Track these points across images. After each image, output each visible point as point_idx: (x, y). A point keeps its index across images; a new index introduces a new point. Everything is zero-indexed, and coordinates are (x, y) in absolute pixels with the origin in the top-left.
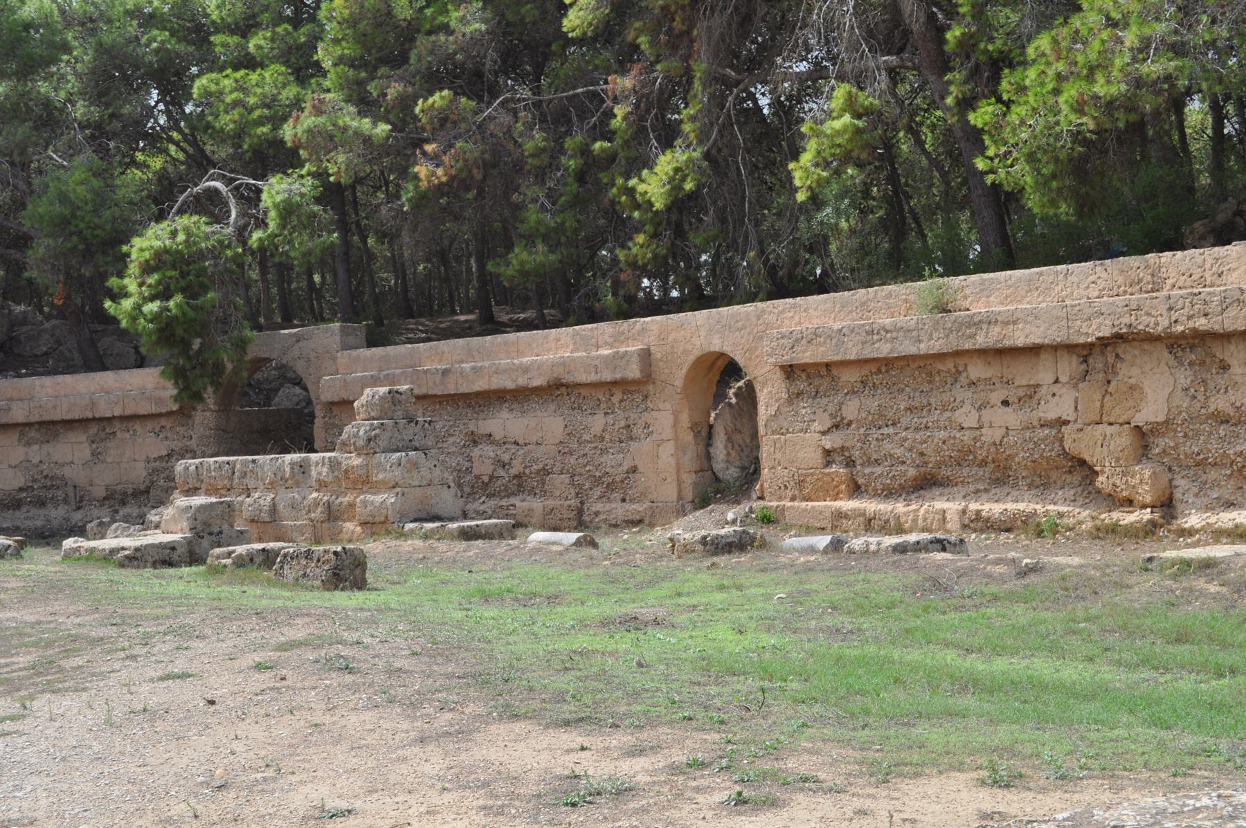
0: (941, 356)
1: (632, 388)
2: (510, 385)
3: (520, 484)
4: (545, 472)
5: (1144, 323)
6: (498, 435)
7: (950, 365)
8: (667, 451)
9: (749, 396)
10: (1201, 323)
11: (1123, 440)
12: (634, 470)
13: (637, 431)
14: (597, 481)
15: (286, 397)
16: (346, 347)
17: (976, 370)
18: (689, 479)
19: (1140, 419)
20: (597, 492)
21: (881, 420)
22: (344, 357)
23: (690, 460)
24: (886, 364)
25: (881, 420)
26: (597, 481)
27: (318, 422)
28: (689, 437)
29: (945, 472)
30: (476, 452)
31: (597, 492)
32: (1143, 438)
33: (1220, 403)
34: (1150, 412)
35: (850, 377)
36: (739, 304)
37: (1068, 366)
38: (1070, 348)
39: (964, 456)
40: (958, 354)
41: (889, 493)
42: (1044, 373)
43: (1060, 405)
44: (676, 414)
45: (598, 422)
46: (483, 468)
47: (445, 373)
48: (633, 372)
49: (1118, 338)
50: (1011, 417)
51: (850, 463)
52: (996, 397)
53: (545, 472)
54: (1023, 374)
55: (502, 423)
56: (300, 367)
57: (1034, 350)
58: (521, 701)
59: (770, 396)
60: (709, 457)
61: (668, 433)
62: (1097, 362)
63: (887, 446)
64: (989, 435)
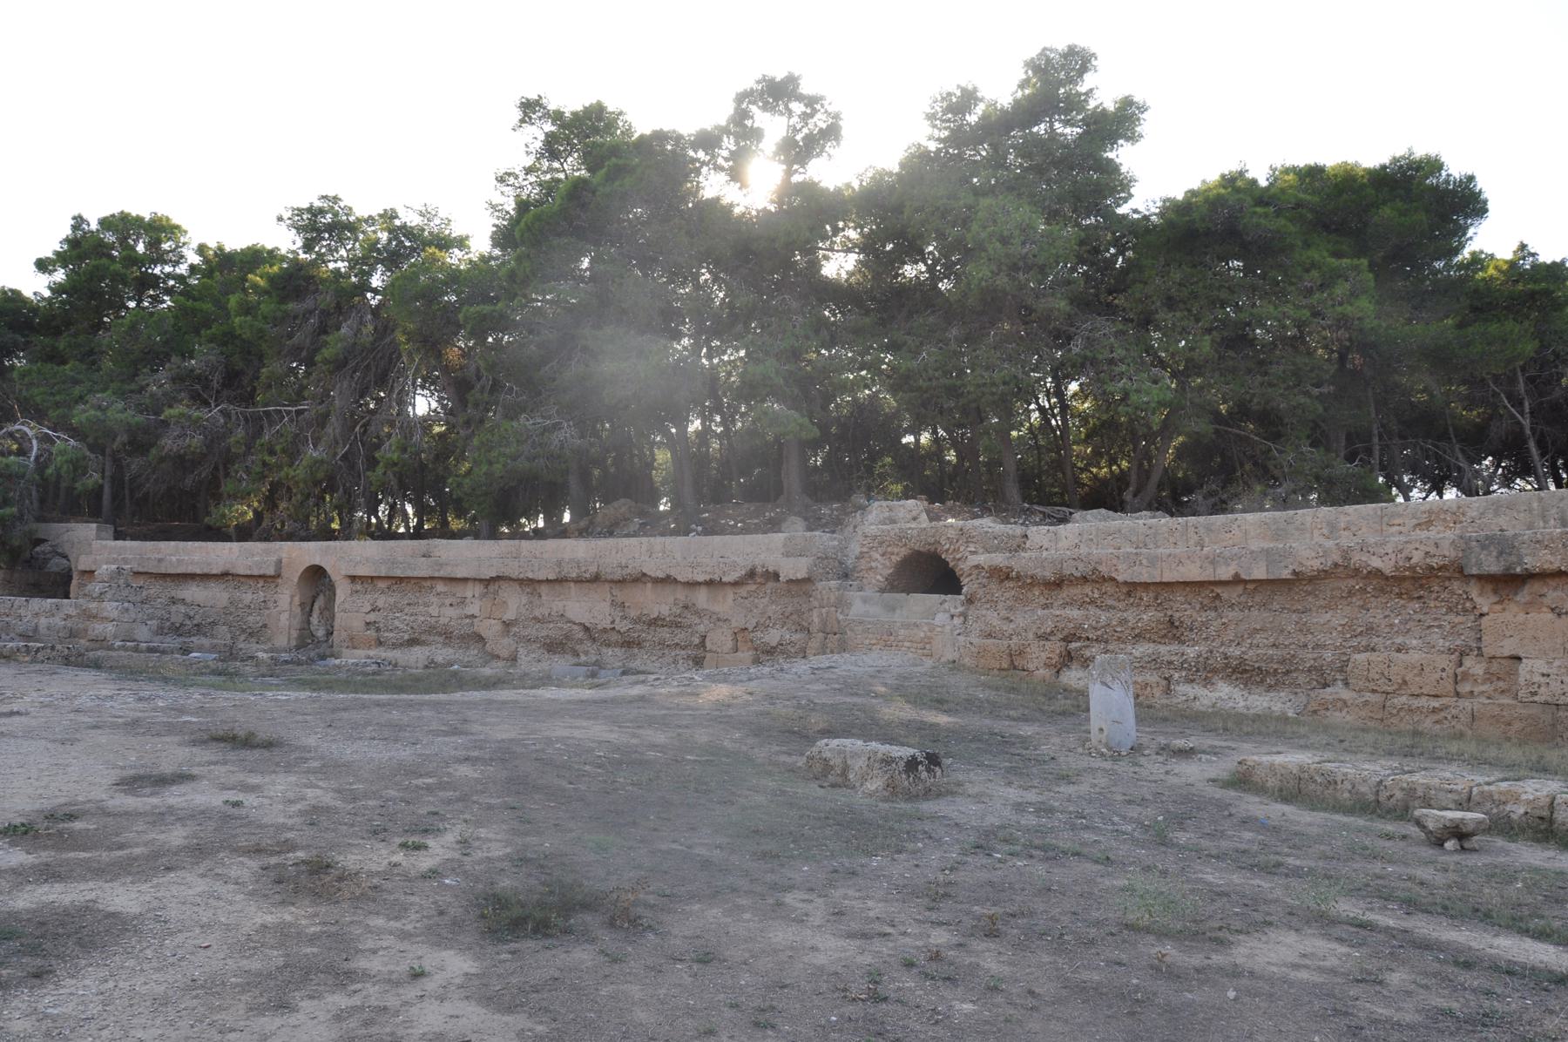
0: (424, 579)
1: (271, 579)
2: (198, 571)
3: (199, 629)
4: (214, 623)
5: (508, 572)
6: (189, 600)
7: (428, 583)
8: (284, 617)
9: (331, 588)
10: (530, 575)
11: (497, 627)
12: (265, 626)
13: (271, 604)
14: (244, 631)
15: (56, 564)
16: (98, 538)
17: (440, 587)
18: (295, 634)
19: (505, 618)
20: (243, 637)
21: (395, 608)
22: (97, 544)
23: (296, 623)
24: (401, 579)
25: (395, 608)
26: (244, 631)
27: (74, 582)
28: (298, 610)
29: (424, 637)
30: (173, 608)
31: (243, 637)
32: (507, 625)
33: (537, 613)
34: (510, 615)
35: (382, 585)
36: (260, 540)
37: (479, 589)
38: (481, 580)
39: (431, 630)
40: (432, 578)
41: (394, 646)
42: (470, 591)
43: (473, 609)
44: (292, 597)
45: (248, 597)
46: (177, 619)
47: (160, 560)
48: (271, 571)
49: (498, 578)
50: (451, 612)
51: (378, 630)
52: (448, 602)
53: (214, 623)
54: (460, 590)
55: (193, 593)
56: (66, 549)
57: (465, 580)
58: (53, 648)
59: (342, 591)
60: (309, 623)
61: (286, 606)
62: (492, 588)
63: (397, 623)
64: (443, 620)
